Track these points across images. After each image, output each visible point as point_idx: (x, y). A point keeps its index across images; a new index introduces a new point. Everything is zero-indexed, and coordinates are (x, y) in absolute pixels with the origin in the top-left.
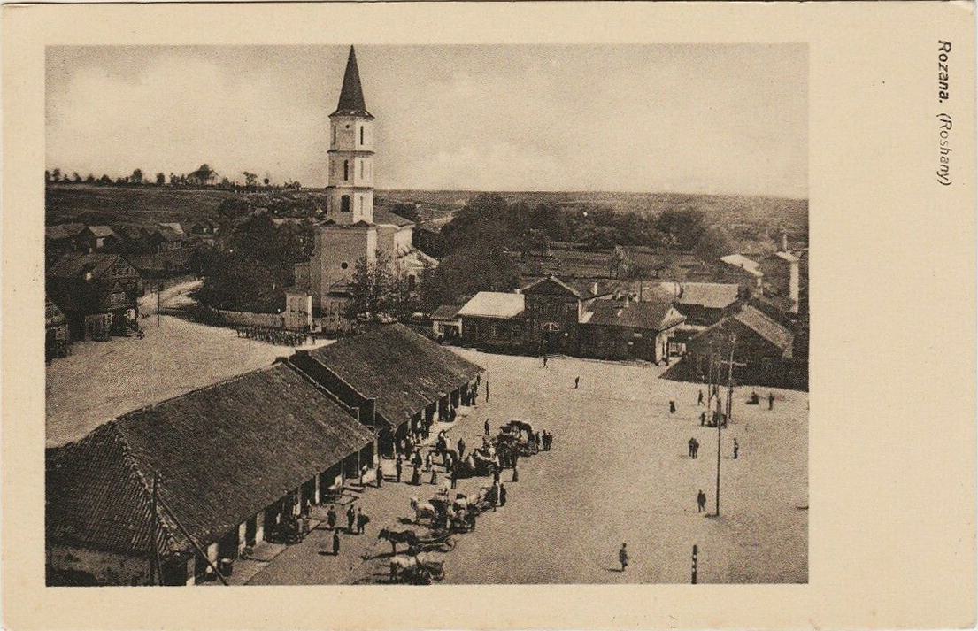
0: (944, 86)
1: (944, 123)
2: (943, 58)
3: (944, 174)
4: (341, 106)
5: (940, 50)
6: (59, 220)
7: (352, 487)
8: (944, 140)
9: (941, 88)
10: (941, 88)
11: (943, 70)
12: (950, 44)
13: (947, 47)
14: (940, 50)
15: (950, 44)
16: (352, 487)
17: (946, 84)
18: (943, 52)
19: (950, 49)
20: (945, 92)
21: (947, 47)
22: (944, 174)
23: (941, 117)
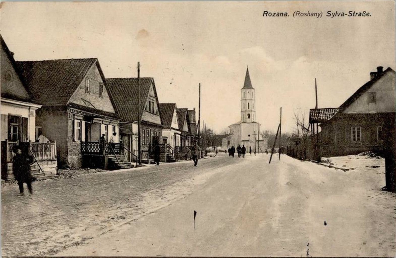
0: (282, 14)
1: (297, 14)
2: (270, 14)
3: (195, 213)
4: (244, 86)
5: (267, 16)
6: (92, 210)
7: (313, 131)
8: (304, 15)
9: (282, 16)
10: (282, 16)
11: (275, 15)
12: (265, 12)
13: (364, 12)
14: (267, 16)
15: (265, 12)
16: (313, 131)
17: (315, 13)
18: (300, 14)
19: (299, 12)
20: (284, 14)
21: (364, 12)
22: (195, 213)
23: (321, 13)
